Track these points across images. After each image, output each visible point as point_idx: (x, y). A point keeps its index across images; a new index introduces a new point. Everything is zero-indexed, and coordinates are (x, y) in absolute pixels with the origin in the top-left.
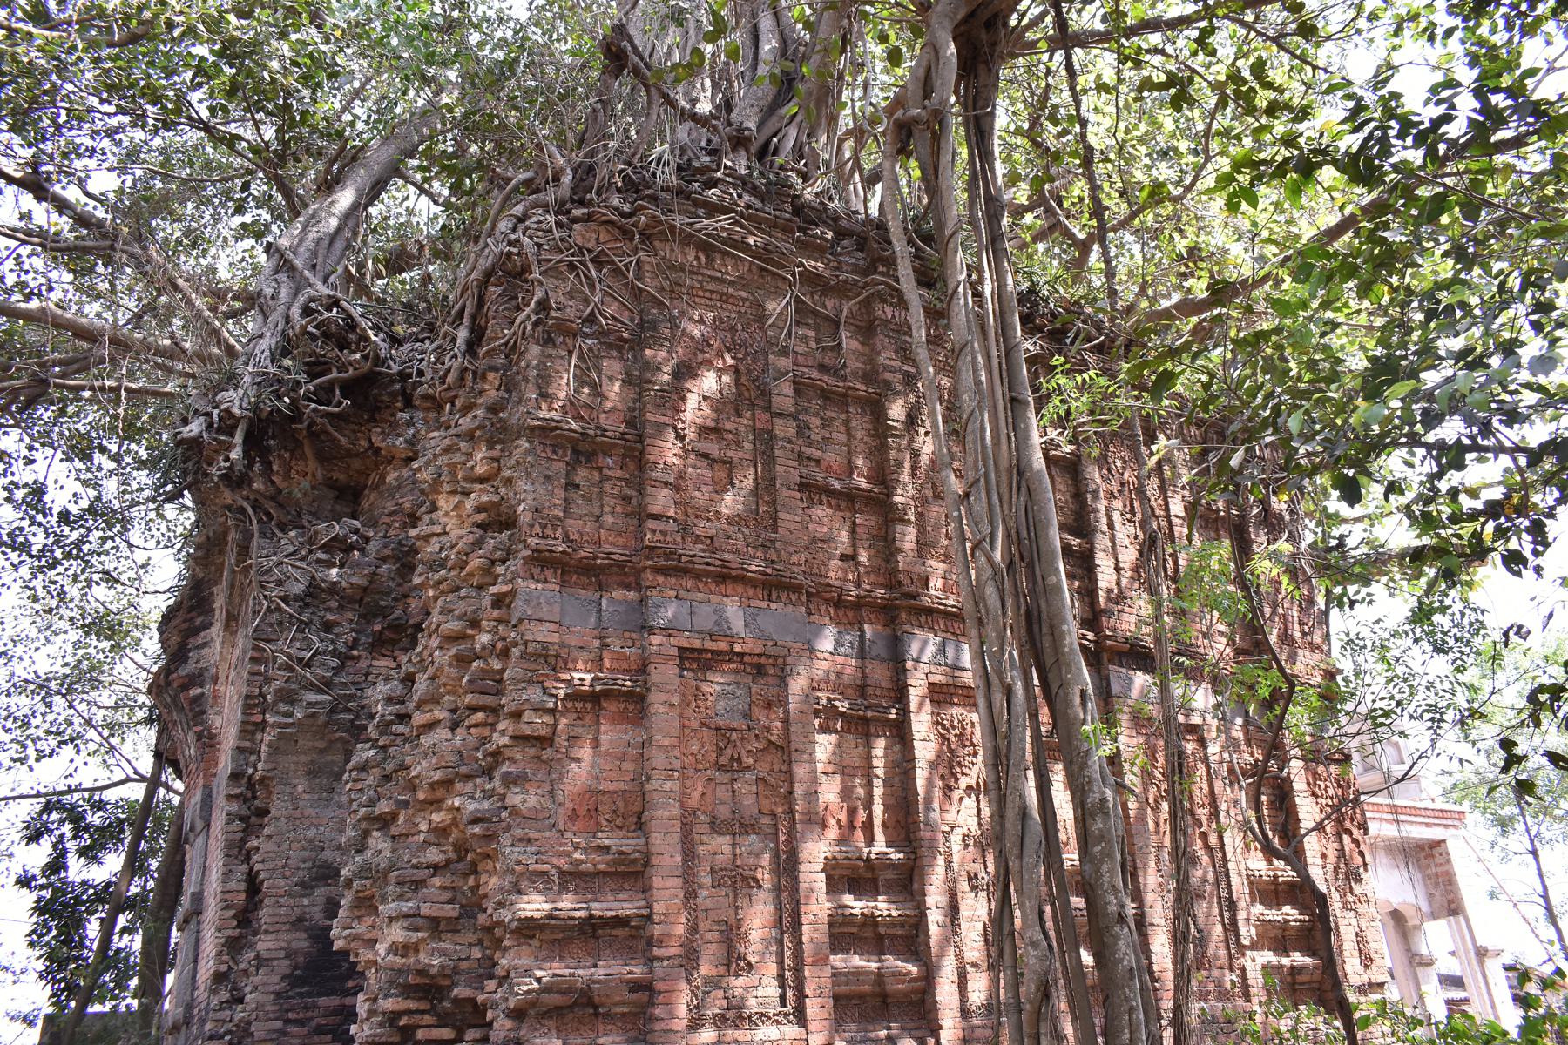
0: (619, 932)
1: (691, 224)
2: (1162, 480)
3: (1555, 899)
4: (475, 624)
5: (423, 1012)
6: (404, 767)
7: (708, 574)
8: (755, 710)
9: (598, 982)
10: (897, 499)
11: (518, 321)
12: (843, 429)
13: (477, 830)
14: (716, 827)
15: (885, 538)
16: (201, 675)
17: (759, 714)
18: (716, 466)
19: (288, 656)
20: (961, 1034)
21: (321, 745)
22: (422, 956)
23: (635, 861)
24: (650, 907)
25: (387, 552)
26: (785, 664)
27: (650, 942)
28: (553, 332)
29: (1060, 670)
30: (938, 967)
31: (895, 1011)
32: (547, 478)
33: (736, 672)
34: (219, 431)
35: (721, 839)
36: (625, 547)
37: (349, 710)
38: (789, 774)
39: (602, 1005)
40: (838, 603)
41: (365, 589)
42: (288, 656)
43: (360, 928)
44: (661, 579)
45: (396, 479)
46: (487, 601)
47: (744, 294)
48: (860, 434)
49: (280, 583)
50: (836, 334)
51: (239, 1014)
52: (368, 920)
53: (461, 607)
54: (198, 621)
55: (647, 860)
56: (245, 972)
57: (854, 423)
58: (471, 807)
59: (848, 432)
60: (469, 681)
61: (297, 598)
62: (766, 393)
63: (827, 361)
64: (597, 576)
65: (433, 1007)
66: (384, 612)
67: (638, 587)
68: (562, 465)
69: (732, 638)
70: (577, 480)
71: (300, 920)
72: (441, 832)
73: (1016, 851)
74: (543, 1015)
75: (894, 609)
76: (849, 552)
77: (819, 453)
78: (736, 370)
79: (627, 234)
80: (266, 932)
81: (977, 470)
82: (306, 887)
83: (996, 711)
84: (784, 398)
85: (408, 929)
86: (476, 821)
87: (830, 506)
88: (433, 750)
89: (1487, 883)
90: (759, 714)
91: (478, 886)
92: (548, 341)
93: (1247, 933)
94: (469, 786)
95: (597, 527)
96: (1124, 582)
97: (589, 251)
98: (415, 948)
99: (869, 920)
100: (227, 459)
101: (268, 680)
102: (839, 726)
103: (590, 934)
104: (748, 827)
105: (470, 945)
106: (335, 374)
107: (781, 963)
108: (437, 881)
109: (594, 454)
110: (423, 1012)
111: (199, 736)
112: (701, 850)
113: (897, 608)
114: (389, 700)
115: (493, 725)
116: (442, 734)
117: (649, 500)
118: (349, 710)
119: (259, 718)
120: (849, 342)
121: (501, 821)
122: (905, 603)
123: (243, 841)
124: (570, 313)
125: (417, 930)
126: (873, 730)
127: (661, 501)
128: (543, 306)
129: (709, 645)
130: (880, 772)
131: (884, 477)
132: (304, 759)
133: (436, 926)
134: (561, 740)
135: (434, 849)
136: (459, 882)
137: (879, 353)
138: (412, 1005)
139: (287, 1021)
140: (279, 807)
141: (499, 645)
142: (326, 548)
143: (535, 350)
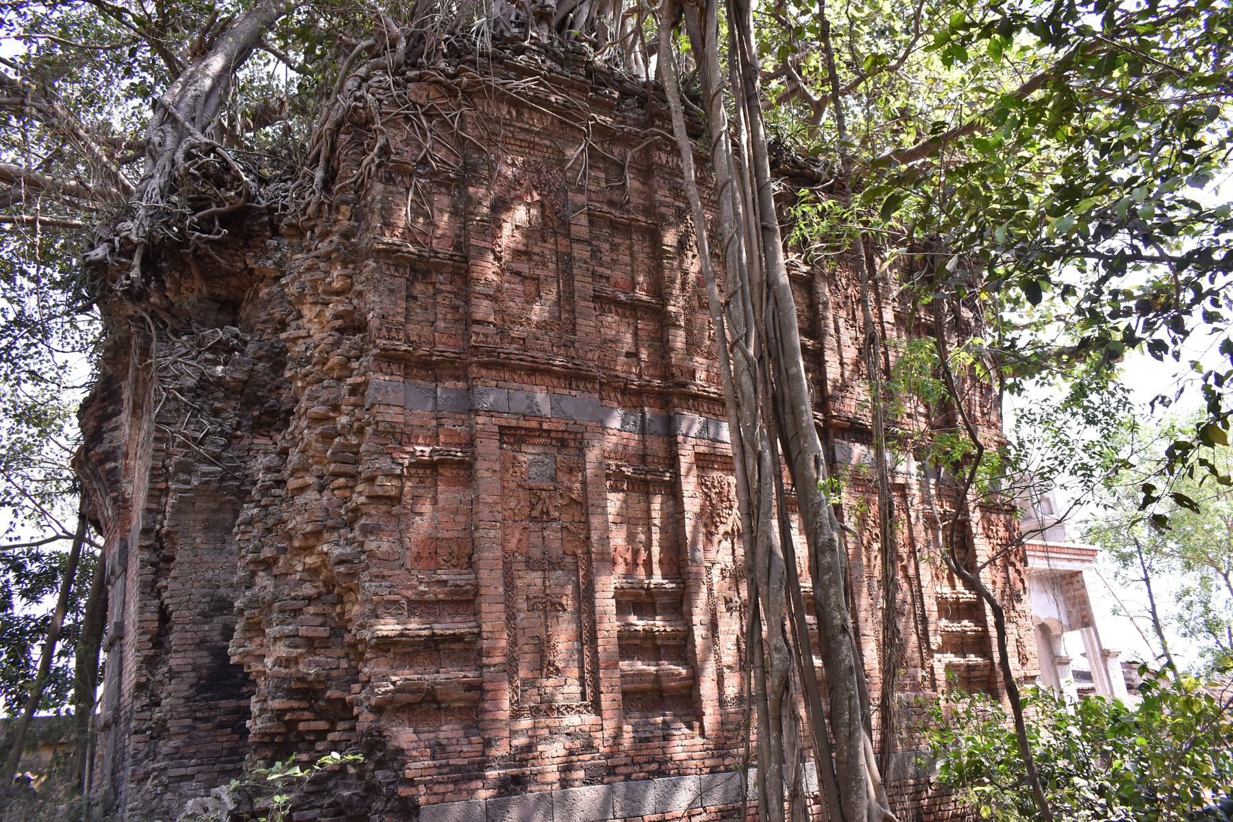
0: (456, 646)
1: (504, 84)
2: (877, 294)
3: (1159, 616)
4: (336, 408)
5: (303, 709)
6: (282, 522)
7: (521, 368)
8: (560, 474)
9: (440, 684)
10: (671, 308)
11: (364, 163)
12: (627, 252)
13: (342, 569)
14: (530, 565)
15: (661, 340)
16: (114, 452)
17: (563, 478)
18: (527, 282)
19: (185, 436)
20: (719, 718)
21: (213, 505)
22: (301, 667)
23: (467, 592)
24: (479, 626)
25: (262, 353)
26: (583, 438)
27: (480, 653)
28: (394, 172)
29: (799, 440)
30: (702, 669)
31: (669, 702)
32: (391, 291)
33: (544, 445)
34: (120, 254)
35: (534, 574)
36: (454, 346)
37: (236, 479)
38: (587, 525)
39: (444, 702)
40: (625, 391)
41: (245, 382)
42: (185, 436)
43: (251, 647)
44: (484, 372)
45: (268, 294)
46: (345, 390)
47: (547, 143)
48: (641, 257)
49: (176, 378)
50: (621, 176)
51: (157, 714)
52: (258, 641)
53: (324, 395)
54: (110, 410)
55: (477, 590)
56: (161, 682)
57: (636, 248)
58: (337, 551)
59: (632, 255)
60: (332, 453)
61: (190, 390)
62: (566, 224)
63: (615, 197)
64: (433, 370)
65: (311, 706)
66: (260, 401)
67: (466, 378)
68: (403, 280)
69: (541, 418)
70: (415, 293)
71: (203, 641)
72: (313, 572)
73: (764, 580)
74: (398, 710)
75: (667, 395)
76: (633, 350)
77: (608, 272)
78: (541, 205)
79: (452, 93)
80: (176, 651)
81: (736, 283)
82: (206, 616)
83: (749, 473)
84: (581, 226)
85: (289, 646)
86: (341, 562)
87: (617, 314)
88: (305, 508)
89: (1110, 603)
90: (563, 478)
91: (343, 613)
92: (389, 180)
93: (936, 641)
94: (335, 536)
95: (433, 332)
96: (847, 374)
97: (422, 106)
98: (296, 661)
99: (649, 634)
100: (128, 278)
101: (169, 455)
102: (625, 487)
103: (433, 647)
104: (555, 565)
105: (339, 658)
106: (214, 208)
107: (581, 668)
108: (311, 610)
109: (429, 272)
110: (303, 709)
111: (115, 500)
112: (519, 583)
113: (670, 394)
114: (268, 469)
115: (352, 488)
116: (312, 495)
117: (473, 309)
118: (236, 479)
119: (163, 486)
120: (632, 182)
121: (361, 562)
122: (676, 390)
123: (155, 581)
124: (407, 157)
125: (297, 647)
126: (651, 489)
127: (483, 309)
128: (385, 151)
129: (523, 424)
130: (657, 522)
131: (660, 292)
132: (200, 517)
133: (311, 644)
134: (407, 499)
135: (308, 585)
136: (328, 610)
137: (656, 192)
138: (295, 704)
139: (196, 719)
140: (182, 555)
141: (356, 425)
142: (212, 349)
143: (379, 187)
